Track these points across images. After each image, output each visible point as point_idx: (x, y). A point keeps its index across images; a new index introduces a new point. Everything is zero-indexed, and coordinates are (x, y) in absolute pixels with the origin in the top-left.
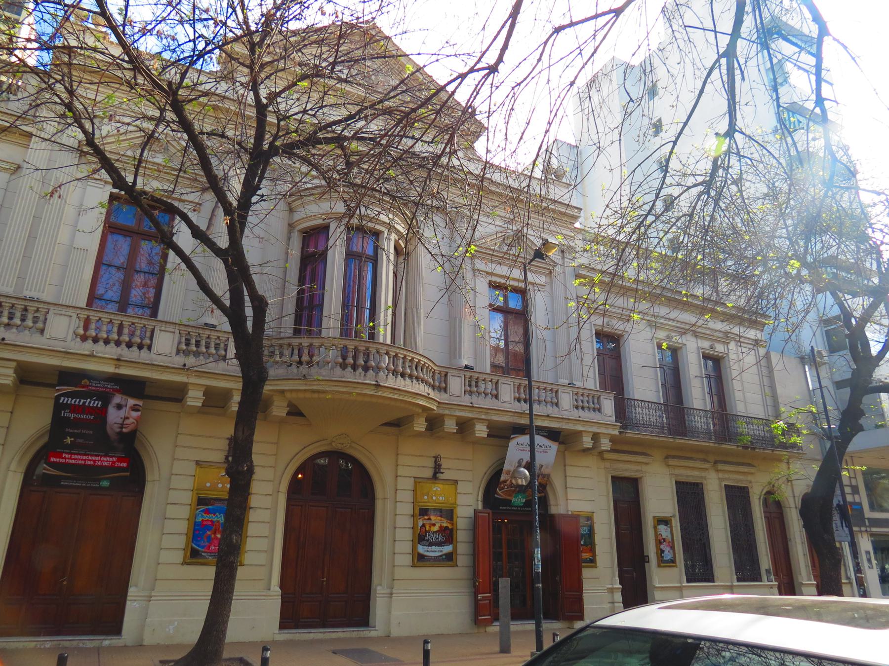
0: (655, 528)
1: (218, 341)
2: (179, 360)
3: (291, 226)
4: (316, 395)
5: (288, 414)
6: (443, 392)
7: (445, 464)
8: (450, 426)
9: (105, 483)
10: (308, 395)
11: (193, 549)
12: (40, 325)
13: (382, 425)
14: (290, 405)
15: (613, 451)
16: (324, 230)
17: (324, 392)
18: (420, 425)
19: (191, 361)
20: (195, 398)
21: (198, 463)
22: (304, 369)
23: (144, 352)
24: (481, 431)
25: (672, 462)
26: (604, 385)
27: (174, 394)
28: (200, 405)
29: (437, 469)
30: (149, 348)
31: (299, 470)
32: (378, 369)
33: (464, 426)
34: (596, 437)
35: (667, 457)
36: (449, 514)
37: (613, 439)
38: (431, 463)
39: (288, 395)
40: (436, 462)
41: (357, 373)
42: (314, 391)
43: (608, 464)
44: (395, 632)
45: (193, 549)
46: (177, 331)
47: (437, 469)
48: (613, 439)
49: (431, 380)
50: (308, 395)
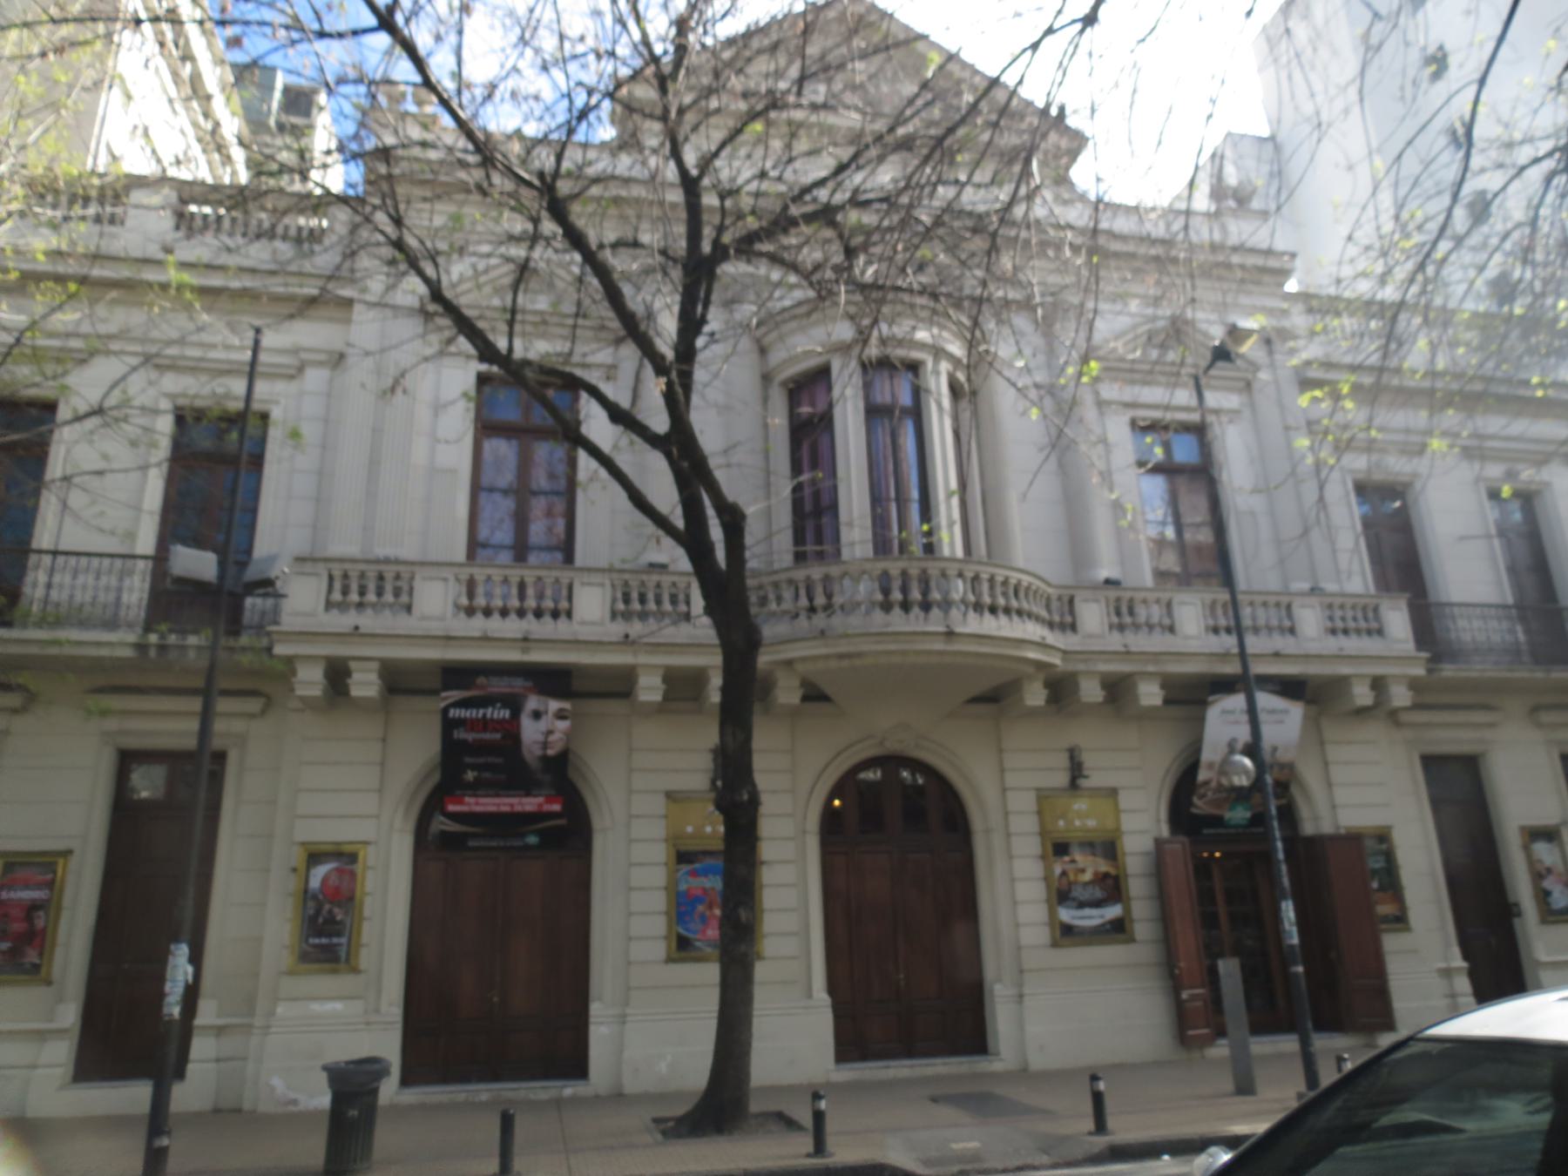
0: (1526, 848)
1: (673, 591)
2: (617, 629)
3: (766, 378)
5: (806, 698)
7: (1088, 760)
8: (1091, 691)
9: (533, 840)
10: (833, 664)
12: (404, 599)
15: (1417, 707)
16: (822, 374)
17: (859, 655)
18: (1035, 696)
19: (636, 628)
20: (650, 689)
21: (670, 796)
22: (820, 620)
23: (562, 623)
24: (1150, 694)
25: (1545, 717)
26: (1384, 583)
27: (618, 686)
29: (1076, 770)
30: (569, 614)
31: (835, 792)
32: (946, 605)
33: (1118, 690)
34: (1378, 684)
35: (1535, 709)
36: (1109, 848)
37: (1414, 685)
38: (1063, 760)
40: (1072, 758)
42: (841, 656)
44: (1037, 1062)
46: (608, 582)
47: (1076, 770)
48: (1414, 685)
49: (1044, 613)
50: (833, 664)
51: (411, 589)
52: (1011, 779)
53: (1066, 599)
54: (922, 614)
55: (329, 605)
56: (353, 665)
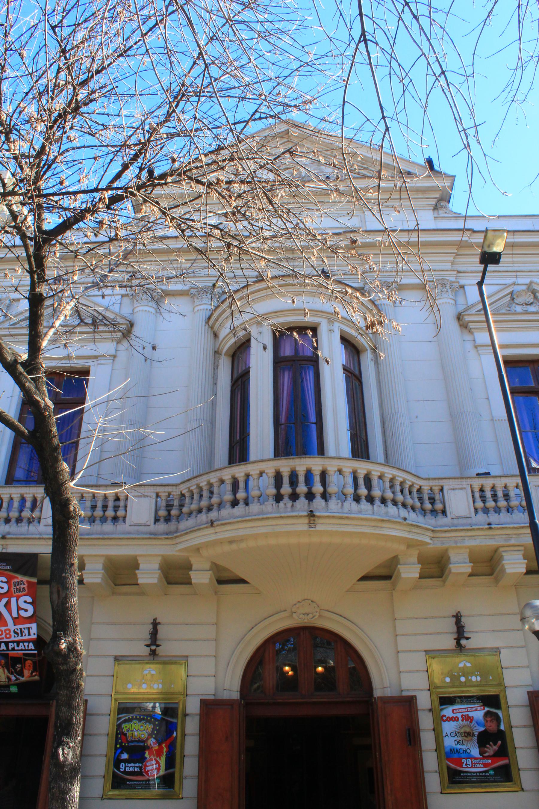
4: (234, 546)
6: (440, 515)
10: (227, 548)
11: (449, 768)
13: (365, 578)
14: (216, 567)
21: (117, 659)
28: (417, 575)
29: (460, 633)
33: (488, 565)
36: (492, 701)
39: (204, 552)
41: (281, 504)
42: (231, 542)
45: (449, 768)
47: (460, 633)
51: (126, 507)
52: (403, 643)
53: (436, 489)
54: (290, 503)
55: (476, 510)
56: (138, 558)
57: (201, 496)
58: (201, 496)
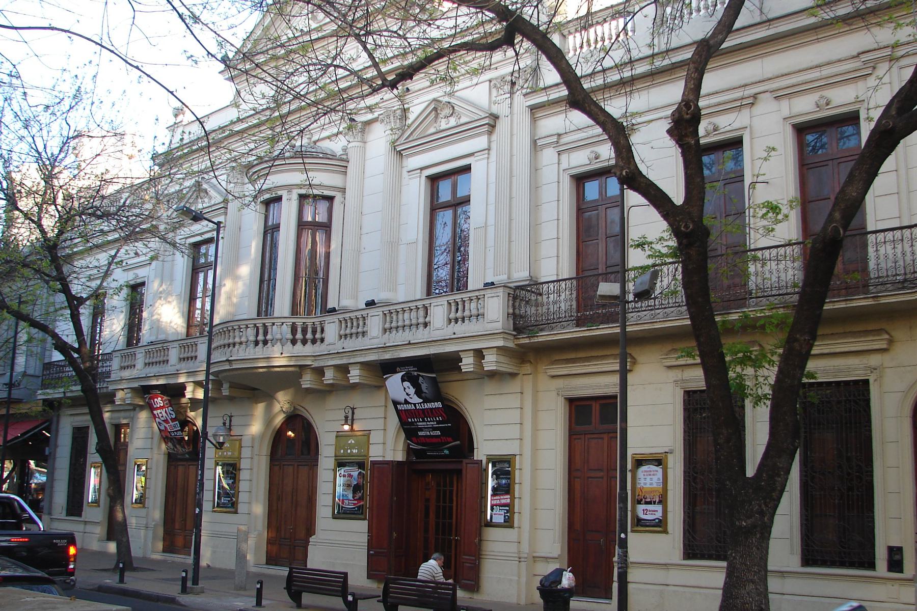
43: (560, 383)
57: (457, 310)
58: (457, 310)
